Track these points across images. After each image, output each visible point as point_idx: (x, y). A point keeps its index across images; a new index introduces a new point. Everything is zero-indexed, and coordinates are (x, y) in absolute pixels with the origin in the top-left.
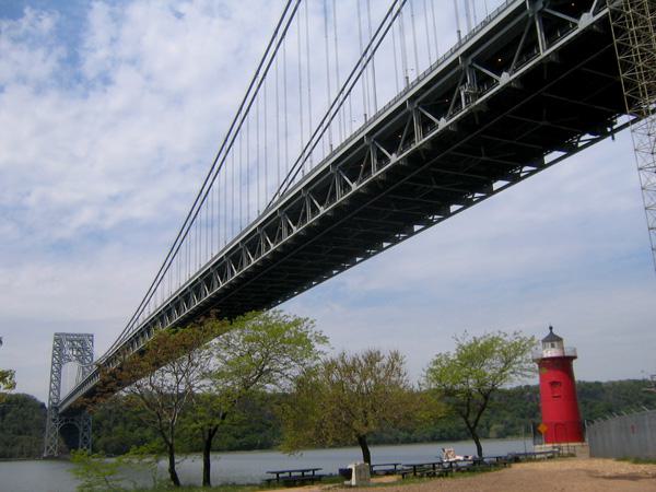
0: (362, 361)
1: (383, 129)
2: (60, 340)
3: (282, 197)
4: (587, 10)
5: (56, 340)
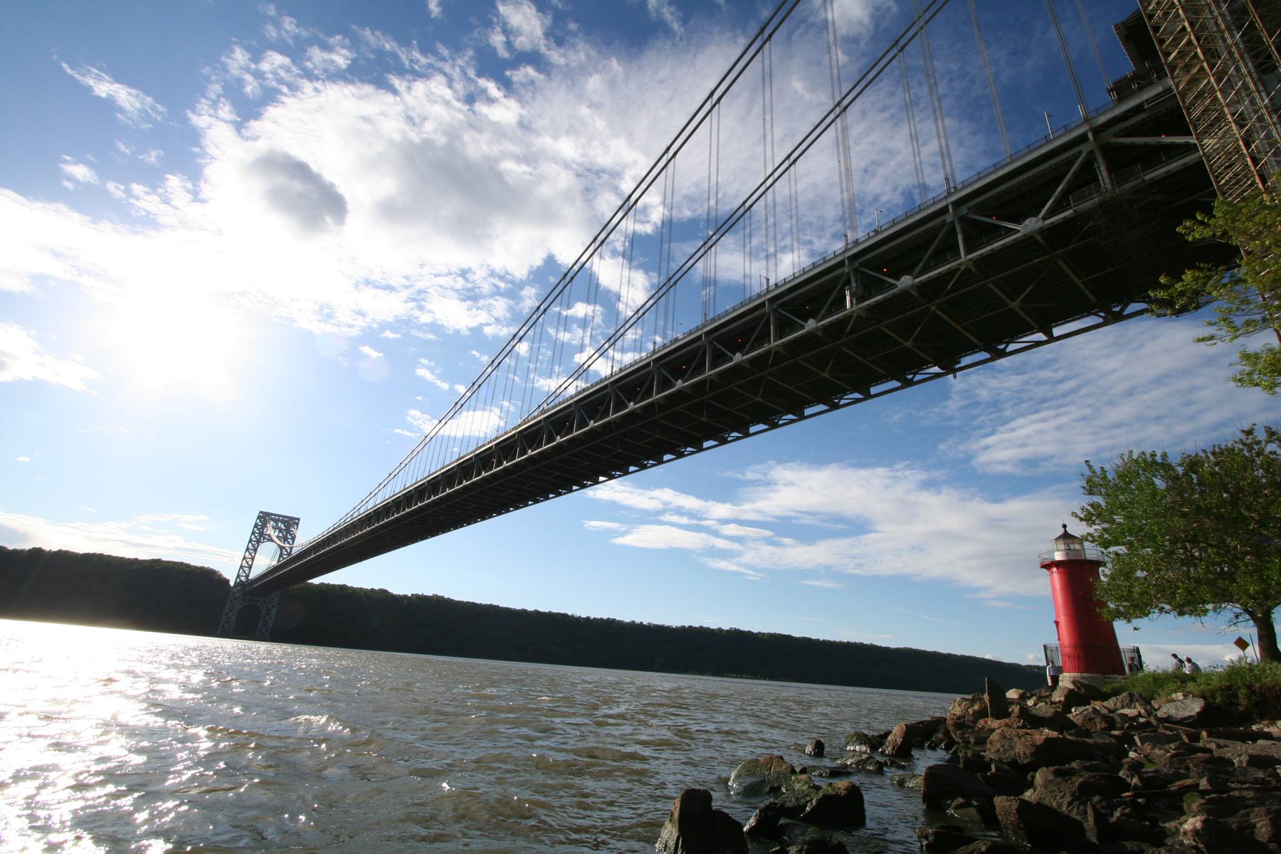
0: (1089, 508)
1: (890, 245)
2: (264, 518)
3: (334, 529)
4: (1035, 214)
5: (259, 518)
